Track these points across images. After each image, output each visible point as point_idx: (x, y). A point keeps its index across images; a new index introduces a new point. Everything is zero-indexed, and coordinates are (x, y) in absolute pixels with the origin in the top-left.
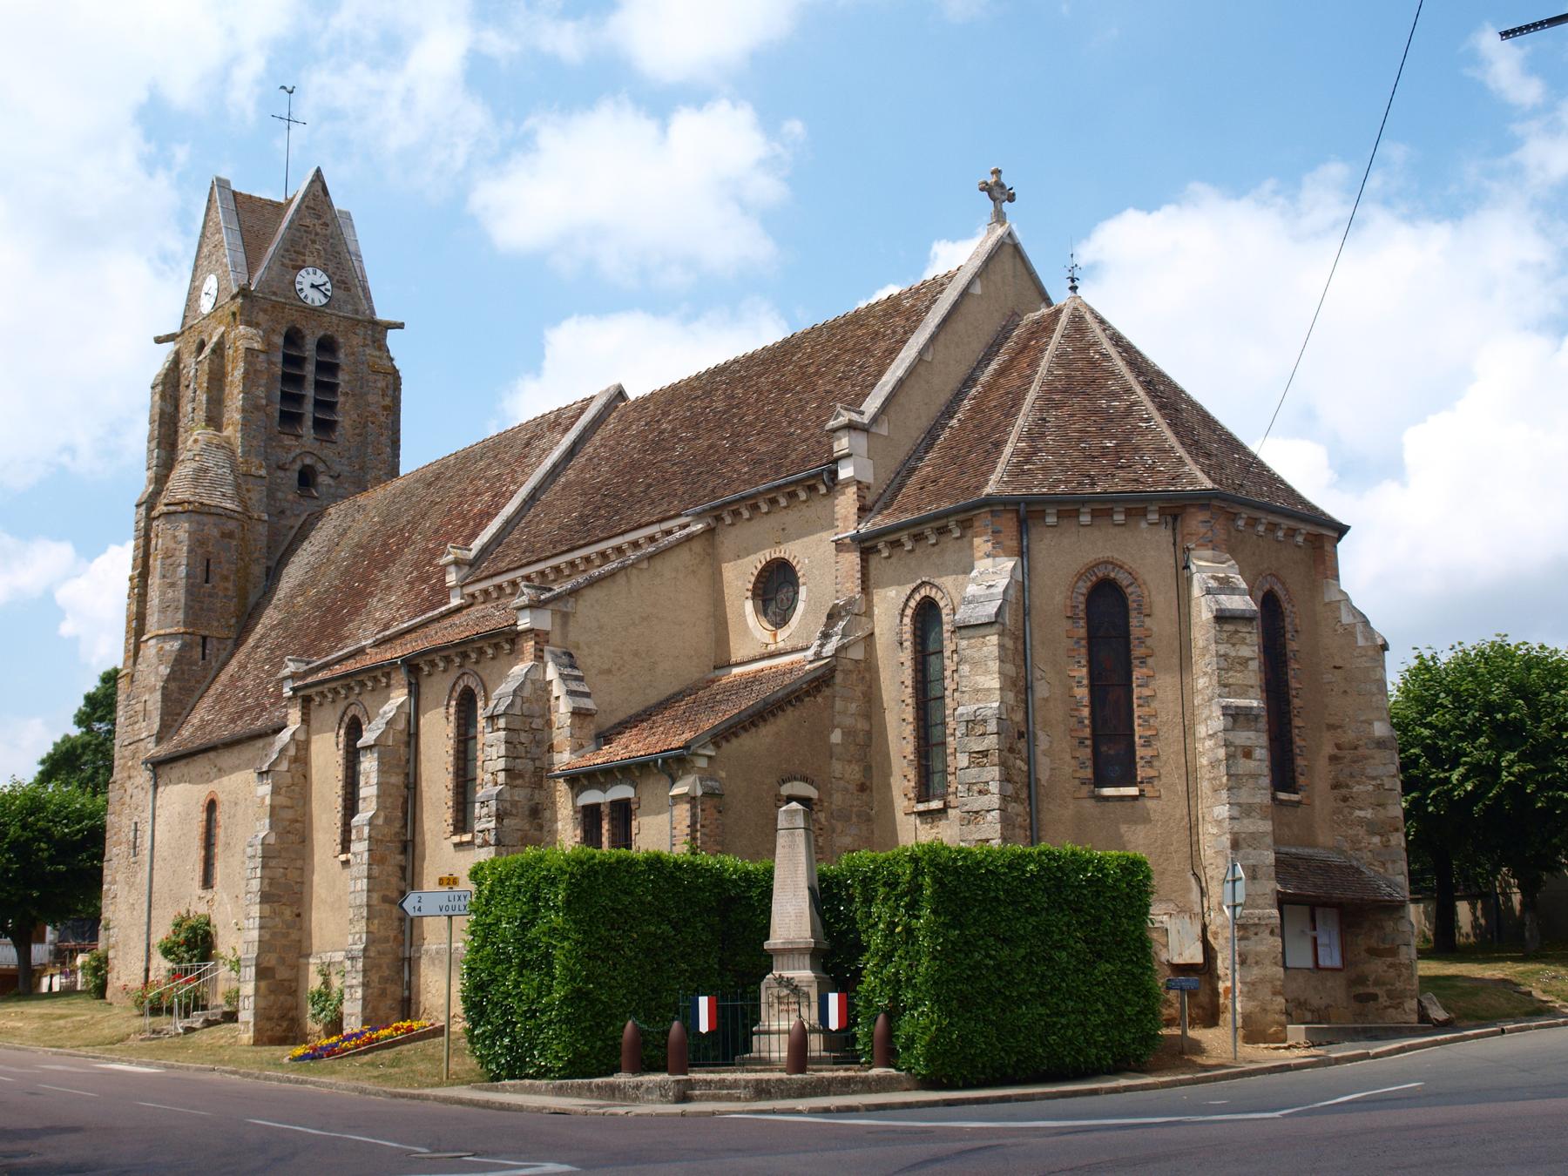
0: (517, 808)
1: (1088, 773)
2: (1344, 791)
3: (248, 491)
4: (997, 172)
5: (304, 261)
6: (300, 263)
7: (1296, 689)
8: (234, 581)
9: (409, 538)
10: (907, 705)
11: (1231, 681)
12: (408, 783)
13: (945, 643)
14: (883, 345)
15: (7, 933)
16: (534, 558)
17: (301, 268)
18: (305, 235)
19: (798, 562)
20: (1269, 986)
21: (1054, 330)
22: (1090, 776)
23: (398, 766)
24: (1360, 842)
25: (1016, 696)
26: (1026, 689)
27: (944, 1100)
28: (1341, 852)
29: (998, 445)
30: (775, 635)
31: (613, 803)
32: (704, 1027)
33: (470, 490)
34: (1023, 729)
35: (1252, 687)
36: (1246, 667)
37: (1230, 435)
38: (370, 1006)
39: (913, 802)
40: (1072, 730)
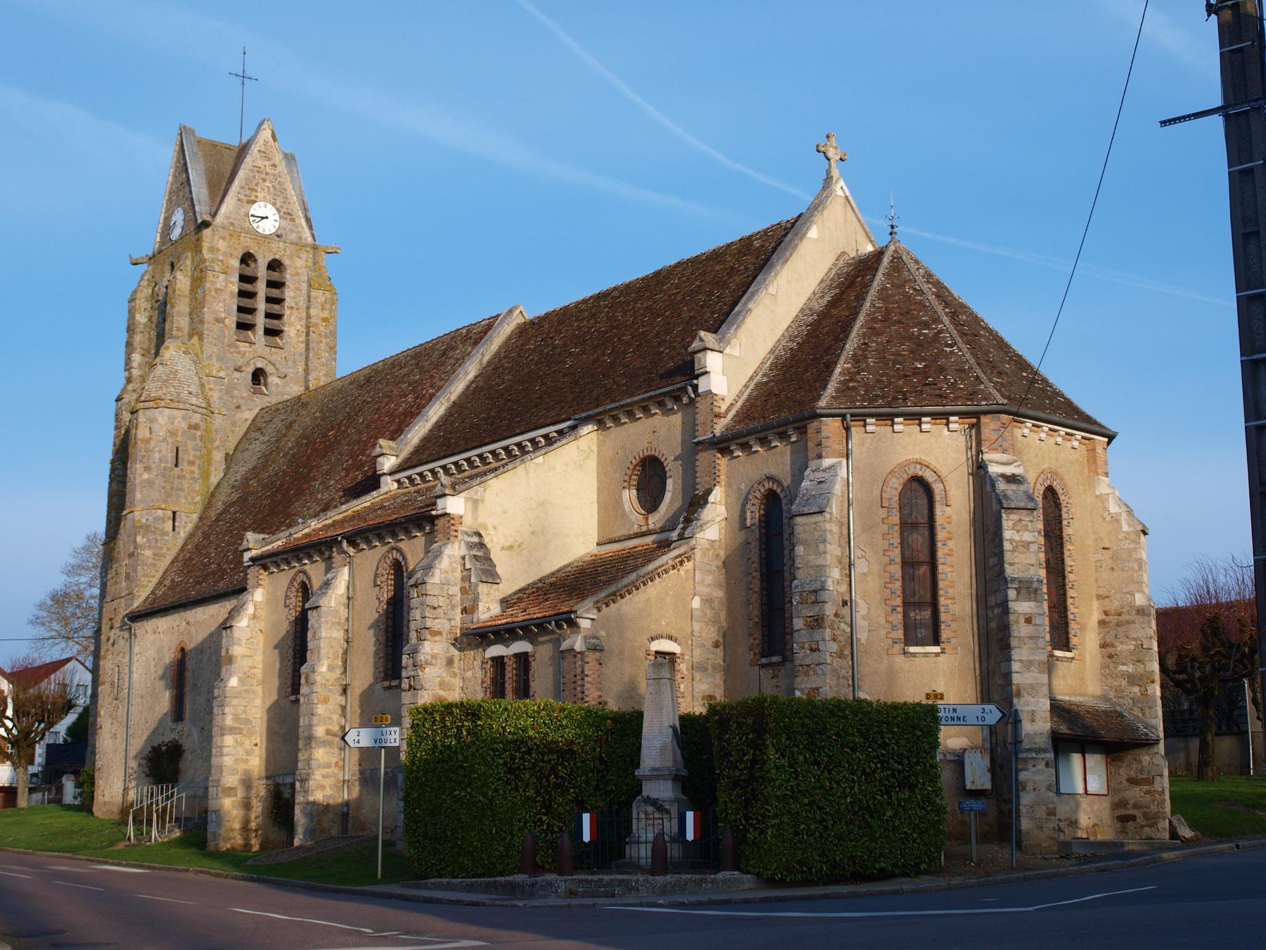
0: (436, 659)
1: (900, 634)
2: (1110, 650)
3: (210, 389)
5: (257, 197)
6: (253, 198)
7: (1071, 566)
8: (199, 465)
9: (345, 431)
11: (1016, 560)
12: (348, 638)
13: (784, 527)
14: (738, 279)
15: (8, 757)
16: (450, 453)
17: (254, 202)
18: (257, 175)
19: (666, 459)
20: (1044, 807)
21: (877, 270)
22: (902, 637)
23: (339, 624)
24: (1123, 691)
25: (841, 572)
26: (850, 566)
27: (776, 897)
29: (830, 367)
30: (647, 519)
31: (516, 655)
32: (586, 837)
33: (396, 392)
34: (847, 598)
35: (1033, 565)
37: (1020, 356)
38: (315, 820)
39: (758, 657)
40: (886, 600)
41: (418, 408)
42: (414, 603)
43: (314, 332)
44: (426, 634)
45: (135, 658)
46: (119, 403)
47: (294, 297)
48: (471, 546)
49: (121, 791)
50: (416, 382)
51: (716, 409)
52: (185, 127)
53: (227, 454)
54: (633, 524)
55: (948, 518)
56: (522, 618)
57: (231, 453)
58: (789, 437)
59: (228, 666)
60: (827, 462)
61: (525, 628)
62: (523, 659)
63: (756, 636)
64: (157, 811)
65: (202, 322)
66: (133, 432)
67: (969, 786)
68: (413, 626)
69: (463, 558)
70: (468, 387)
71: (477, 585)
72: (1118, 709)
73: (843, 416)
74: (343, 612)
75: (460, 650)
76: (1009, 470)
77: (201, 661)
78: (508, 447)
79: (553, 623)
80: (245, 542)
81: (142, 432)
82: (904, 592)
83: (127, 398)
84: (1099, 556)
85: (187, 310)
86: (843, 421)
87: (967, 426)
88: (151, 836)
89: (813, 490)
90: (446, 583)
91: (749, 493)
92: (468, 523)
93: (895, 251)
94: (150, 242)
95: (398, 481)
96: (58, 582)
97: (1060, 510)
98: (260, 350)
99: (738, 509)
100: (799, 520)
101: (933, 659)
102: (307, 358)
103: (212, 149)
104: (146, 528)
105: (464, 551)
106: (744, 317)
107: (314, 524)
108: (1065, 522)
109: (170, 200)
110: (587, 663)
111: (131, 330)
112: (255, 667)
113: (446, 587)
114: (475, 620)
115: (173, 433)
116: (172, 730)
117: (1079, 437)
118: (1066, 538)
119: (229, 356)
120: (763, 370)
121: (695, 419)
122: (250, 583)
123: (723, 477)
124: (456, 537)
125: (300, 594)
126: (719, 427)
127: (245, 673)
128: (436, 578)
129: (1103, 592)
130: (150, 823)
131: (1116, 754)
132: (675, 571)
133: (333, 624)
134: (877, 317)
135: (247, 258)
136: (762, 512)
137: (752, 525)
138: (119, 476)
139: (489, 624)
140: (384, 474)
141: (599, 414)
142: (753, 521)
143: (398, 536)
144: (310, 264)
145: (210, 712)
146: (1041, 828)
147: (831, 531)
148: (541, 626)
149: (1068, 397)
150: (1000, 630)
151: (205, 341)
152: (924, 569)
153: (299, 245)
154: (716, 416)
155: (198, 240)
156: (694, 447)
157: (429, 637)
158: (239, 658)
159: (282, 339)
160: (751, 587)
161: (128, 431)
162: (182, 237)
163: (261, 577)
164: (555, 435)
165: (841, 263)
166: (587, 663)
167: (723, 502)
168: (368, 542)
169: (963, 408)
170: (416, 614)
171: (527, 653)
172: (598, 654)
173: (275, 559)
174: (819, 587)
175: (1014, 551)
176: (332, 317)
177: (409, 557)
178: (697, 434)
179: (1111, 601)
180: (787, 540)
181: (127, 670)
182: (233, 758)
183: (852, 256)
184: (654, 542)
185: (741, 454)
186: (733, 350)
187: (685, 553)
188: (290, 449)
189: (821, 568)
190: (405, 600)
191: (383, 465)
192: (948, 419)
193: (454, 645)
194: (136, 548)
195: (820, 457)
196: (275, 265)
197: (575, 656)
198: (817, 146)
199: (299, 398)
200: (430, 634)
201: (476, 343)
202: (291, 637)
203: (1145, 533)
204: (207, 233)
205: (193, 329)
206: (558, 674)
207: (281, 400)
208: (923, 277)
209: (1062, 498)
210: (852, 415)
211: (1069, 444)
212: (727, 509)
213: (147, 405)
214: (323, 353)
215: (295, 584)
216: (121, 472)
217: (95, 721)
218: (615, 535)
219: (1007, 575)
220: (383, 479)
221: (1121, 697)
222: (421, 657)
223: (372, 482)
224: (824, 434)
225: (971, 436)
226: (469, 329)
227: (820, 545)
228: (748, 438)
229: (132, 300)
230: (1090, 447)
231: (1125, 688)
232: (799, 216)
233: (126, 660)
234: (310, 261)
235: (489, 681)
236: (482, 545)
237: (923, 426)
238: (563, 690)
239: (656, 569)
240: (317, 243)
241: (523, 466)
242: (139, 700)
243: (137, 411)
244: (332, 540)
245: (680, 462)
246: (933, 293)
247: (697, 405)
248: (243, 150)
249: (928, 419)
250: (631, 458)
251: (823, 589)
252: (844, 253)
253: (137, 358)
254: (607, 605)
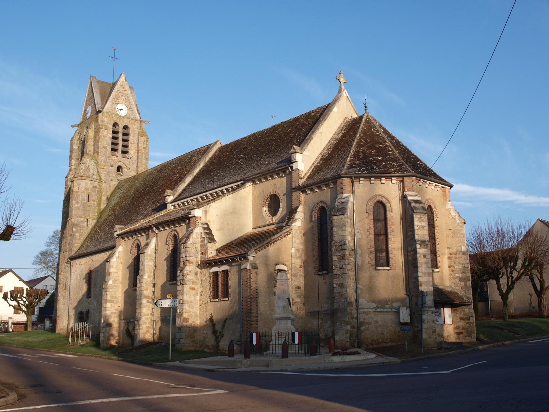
2: (452, 268)
4: (5, 297)
5: (119, 102)
6: (118, 102)
10: (315, 241)
13: (328, 221)
17: (118, 104)
21: (360, 123)
22: (375, 263)
23: (152, 259)
25: (351, 238)
26: (354, 235)
28: (451, 287)
30: (272, 218)
31: (223, 271)
34: (353, 248)
36: (424, 229)
37: (416, 156)
39: (317, 271)
41: (181, 178)
42: (182, 251)
43: (140, 152)
44: (187, 263)
45: (72, 274)
46: (67, 179)
47: (133, 139)
49: (67, 325)
50: (180, 169)
51: (300, 176)
52: (92, 76)
53: (107, 198)
54: (267, 220)
55: (392, 217)
56: (226, 256)
57: (109, 197)
58: (330, 186)
59: (108, 276)
60: (345, 195)
61: (227, 261)
63: (316, 263)
64: (80, 332)
65: (98, 148)
66: (72, 189)
67: (402, 321)
68: (182, 260)
69: (201, 233)
70: (200, 170)
71: (207, 244)
72: (456, 291)
73: (351, 177)
74: (154, 255)
75: (200, 269)
76: (416, 198)
77: (97, 275)
79: (238, 258)
81: (75, 189)
85: (93, 143)
86: (351, 179)
87: (399, 181)
88: (78, 342)
89: (340, 206)
90: (195, 243)
91: (313, 208)
92: (203, 220)
94: (78, 119)
95: (174, 206)
96: (44, 248)
97: (433, 214)
98: (120, 159)
99: (309, 214)
101: (386, 272)
103: (102, 84)
104: (76, 225)
105: (202, 230)
106: (310, 141)
107: (142, 222)
108: (435, 219)
109: (86, 103)
110: (252, 274)
111: (71, 151)
112: (119, 277)
113: (194, 245)
114: (206, 258)
115: (87, 189)
117: (440, 187)
118: (435, 225)
119: (108, 161)
120: (317, 161)
122: (117, 244)
124: (198, 225)
125: (137, 248)
126: (301, 182)
127: (115, 279)
128: (191, 240)
129: (449, 246)
130: (78, 337)
131: (455, 308)
132: (285, 238)
133: (150, 260)
134: (362, 141)
135: (115, 125)
136: (318, 215)
137: (315, 220)
138: (66, 206)
140: (168, 203)
143: (181, 224)
144: (139, 127)
145: (101, 295)
146: (430, 337)
147: (347, 222)
148: (233, 259)
150: (413, 260)
151: (99, 155)
152: (383, 237)
153: (135, 120)
154: (300, 178)
155: (97, 117)
156: (291, 190)
157: (188, 264)
158: (113, 273)
159: (128, 155)
160: (314, 244)
161: (70, 189)
162: (91, 116)
163: (121, 242)
164: (236, 187)
165: (346, 121)
166: (252, 274)
167: (303, 212)
168: (163, 228)
169: (397, 174)
170: (183, 255)
171: (227, 270)
172: (256, 270)
173: (126, 235)
174: (343, 244)
175: (418, 229)
176: (147, 147)
178: (292, 185)
179: (452, 249)
180: (329, 226)
181: (69, 279)
182: (110, 312)
183: (350, 119)
184: (275, 227)
185: (310, 193)
186: (306, 152)
187: (289, 231)
188: (132, 195)
190: (178, 250)
191: (168, 199)
193: (198, 267)
194: (73, 232)
195: (342, 193)
196: (125, 127)
197: (247, 271)
198: (336, 77)
199: (135, 176)
200: (189, 263)
202: (133, 265)
203: (465, 223)
205: (95, 151)
206: (240, 278)
207: (127, 178)
208: (378, 126)
209: (434, 210)
212: (304, 214)
213: (77, 178)
214: (143, 161)
215: (135, 244)
216: (67, 205)
217: (57, 298)
218: (260, 225)
219: (416, 239)
220: (168, 205)
221: (457, 287)
222: (185, 272)
223: (164, 206)
224: (344, 184)
225: (400, 185)
226: (200, 149)
227: (343, 227)
228: (314, 186)
229: (72, 140)
230: (444, 191)
231: (458, 283)
233: (69, 275)
234: (139, 126)
236: (208, 228)
238: (242, 285)
239: (278, 237)
240: (141, 120)
241: (224, 198)
242: (74, 290)
243: (73, 181)
244: (149, 227)
245: (286, 196)
246: (383, 132)
248: (114, 85)
249: (384, 179)
250: (266, 195)
251: (345, 244)
252: (346, 118)
253: (73, 162)
254: (259, 251)
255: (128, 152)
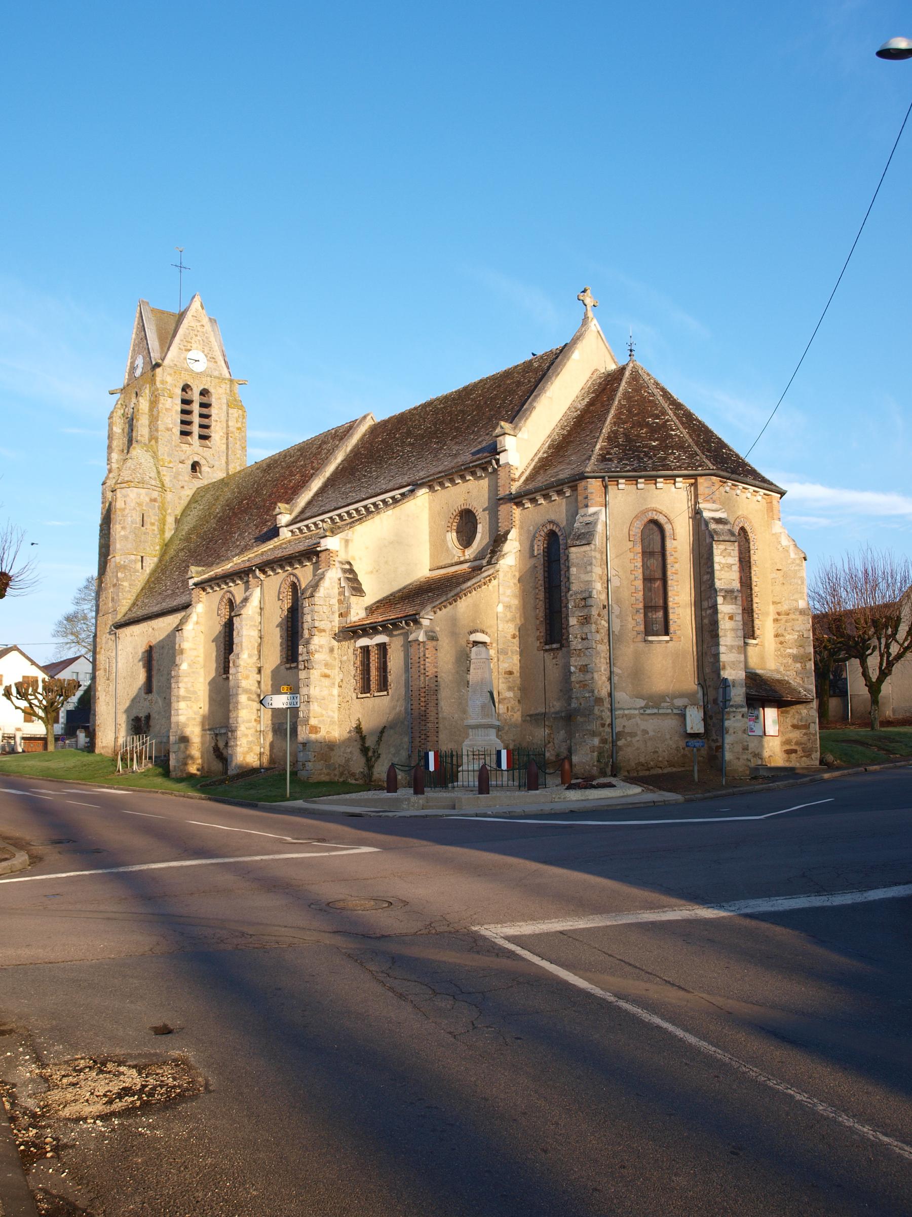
2: (781, 639)
6: (189, 348)
11: (722, 577)
17: (190, 350)
21: (621, 380)
23: (255, 626)
24: (789, 667)
26: (607, 581)
30: (464, 552)
31: (377, 645)
32: (432, 768)
34: (606, 603)
39: (542, 645)
41: (303, 483)
42: (306, 610)
44: (315, 631)
45: (119, 653)
47: (218, 414)
48: (345, 571)
51: (512, 476)
53: (176, 519)
54: (454, 556)
58: (564, 493)
60: (591, 510)
61: (383, 626)
62: (383, 647)
65: (157, 430)
67: (689, 731)
68: (306, 626)
69: (340, 580)
70: (337, 468)
71: (349, 598)
72: (786, 678)
73: (603, 478)
74: (258, 618)
75: (338, 641)
76: (718, 515)
78: (367, 505)
79: (404, 622)
80: (190, 573)
81: (119, 504)
82: (644, 599)
83: (109, 483)
84: (774, 575)
85: (147, 423)
86: (603, 481)
90: (328, 596)
91: (536, 532)
93: (633, 367)
94: (121, 380)
95: (292, 531)
96: (71, 609)
97: (749, 543)
98: (196, 450)
100: (573, 550)
101: (664, 645)
102: (227, 454)
103: (160, 315)
104: (124, 568)
105: (340, 574)
108: (752, 552)
111: (110, 437)
113: (328, 599)
114: (348, 622)
116: (145, 699)
117: (762, 494)
118: (752, 562)
119: (176, 453)
121: (497, 483)
122: (194, 600)
123: (517, 522)
126: (515, 488)
128: (321, 592)
129: (777, 599)
130: (132, 760)
132: (486, 586)
133: (251, 626)
135: (186, 388)
138: (105, 534)
139: (358, 624)
140: (282, 526)
141: (429, 481)
142: (539, 552)
144: (228, 391)
146: (738, 759)
149: (753, 466)
150: (711, 625)
152: (658, 584)
153: (221, 379)
156: (497, 501)
157: (317, 633)
162: (142, 374)
164: (399, 496)
165: (595, 377)
168: (273, 570)
169: (686, 472)
172: (434, 643)
175: (721, 570)
177: (302, 579)
183: (602, 372)
184: (469, 568)
188: (218, 513)
189: (589, 582)
190: (299, 608)
191: (280, 520)
192: (675, 480)
194: (117, 580)
195: (587, 506)
196: (204, 393)
197: (419, 645)
199: (223, 480)
200: (318, 631)
201: (341, 439)
204: (159, 371)
209: (750, 535)
210: (609, 478)
211: (755, 499)
212: (520, 544)
213: (123, 485)
215: (224, 600)
217: (95, 694)
218: (442, 564)
219: (716, 587)
220: (281, 530)
221: (789, 671)
222: (312, 647)
223: (274, 532)
226: (337, 430)
229: (110, 417)
232: (566, 345)
234: (228, 389)
235: (358, 663)
236: (351, 571)
237: (658, 485)
241: (379, 516)
246: (661, 395)
247: (499, 473)
248: (182, 316)
250: (452, 511)
251: (590, 597)
252: (596, 370)
253: (115, 456)
255: (210, 437)
